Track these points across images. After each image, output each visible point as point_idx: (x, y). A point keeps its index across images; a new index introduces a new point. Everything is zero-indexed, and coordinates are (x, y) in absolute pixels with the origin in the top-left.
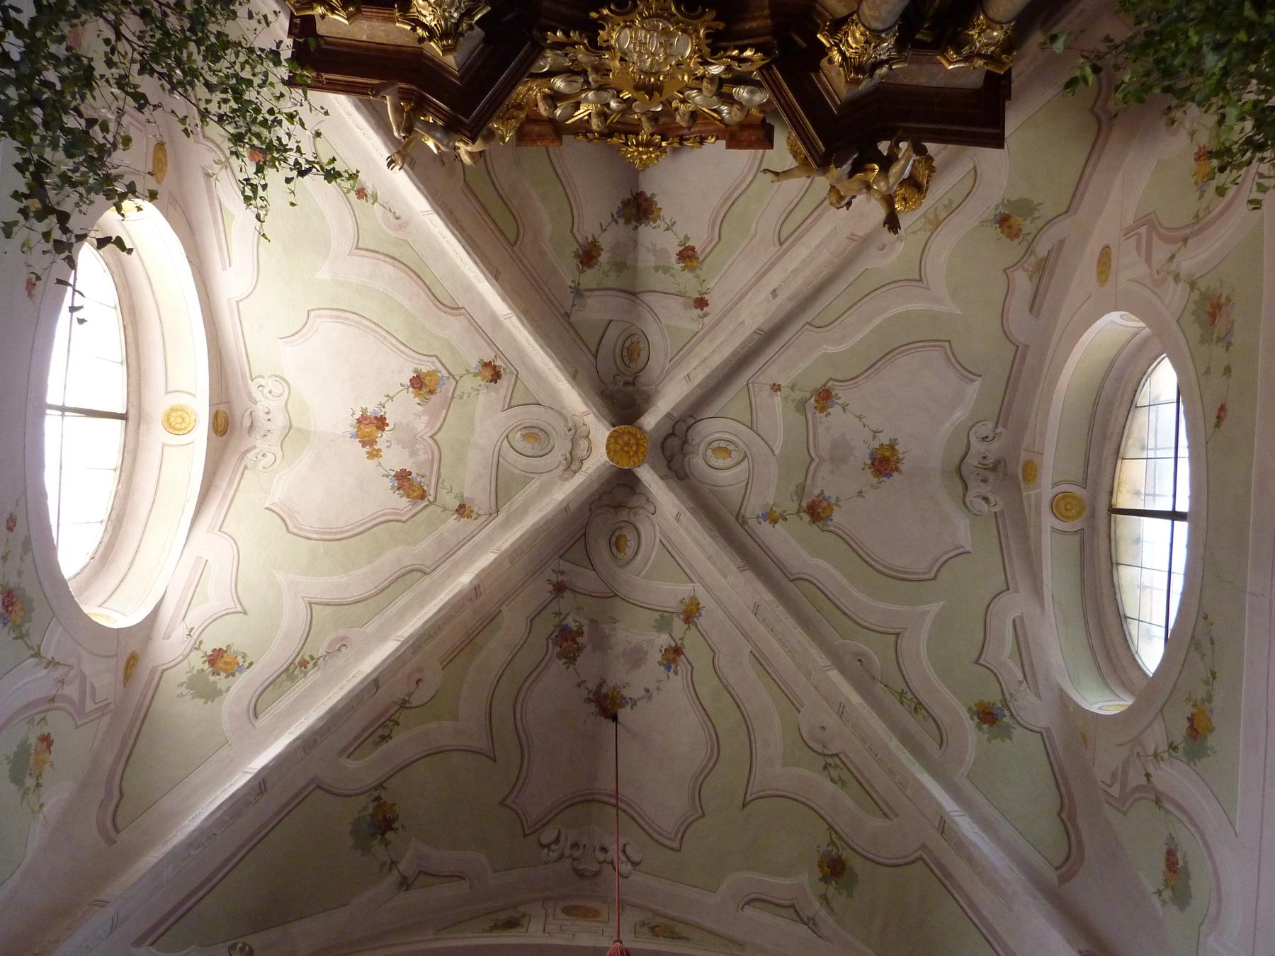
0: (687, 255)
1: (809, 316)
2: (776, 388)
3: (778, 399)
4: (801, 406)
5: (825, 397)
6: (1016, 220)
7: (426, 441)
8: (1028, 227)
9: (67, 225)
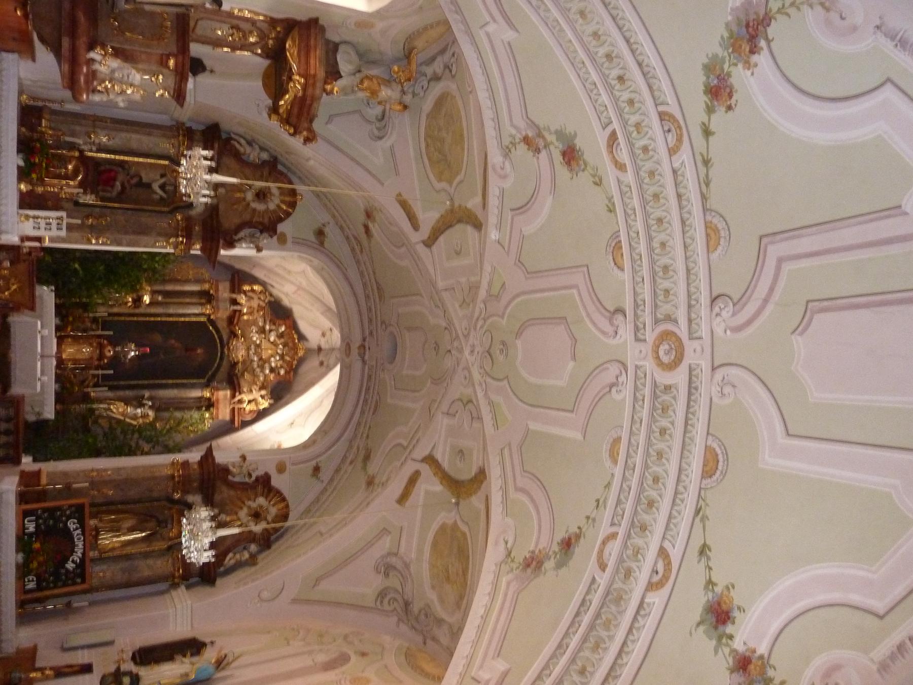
0: (323, 335)
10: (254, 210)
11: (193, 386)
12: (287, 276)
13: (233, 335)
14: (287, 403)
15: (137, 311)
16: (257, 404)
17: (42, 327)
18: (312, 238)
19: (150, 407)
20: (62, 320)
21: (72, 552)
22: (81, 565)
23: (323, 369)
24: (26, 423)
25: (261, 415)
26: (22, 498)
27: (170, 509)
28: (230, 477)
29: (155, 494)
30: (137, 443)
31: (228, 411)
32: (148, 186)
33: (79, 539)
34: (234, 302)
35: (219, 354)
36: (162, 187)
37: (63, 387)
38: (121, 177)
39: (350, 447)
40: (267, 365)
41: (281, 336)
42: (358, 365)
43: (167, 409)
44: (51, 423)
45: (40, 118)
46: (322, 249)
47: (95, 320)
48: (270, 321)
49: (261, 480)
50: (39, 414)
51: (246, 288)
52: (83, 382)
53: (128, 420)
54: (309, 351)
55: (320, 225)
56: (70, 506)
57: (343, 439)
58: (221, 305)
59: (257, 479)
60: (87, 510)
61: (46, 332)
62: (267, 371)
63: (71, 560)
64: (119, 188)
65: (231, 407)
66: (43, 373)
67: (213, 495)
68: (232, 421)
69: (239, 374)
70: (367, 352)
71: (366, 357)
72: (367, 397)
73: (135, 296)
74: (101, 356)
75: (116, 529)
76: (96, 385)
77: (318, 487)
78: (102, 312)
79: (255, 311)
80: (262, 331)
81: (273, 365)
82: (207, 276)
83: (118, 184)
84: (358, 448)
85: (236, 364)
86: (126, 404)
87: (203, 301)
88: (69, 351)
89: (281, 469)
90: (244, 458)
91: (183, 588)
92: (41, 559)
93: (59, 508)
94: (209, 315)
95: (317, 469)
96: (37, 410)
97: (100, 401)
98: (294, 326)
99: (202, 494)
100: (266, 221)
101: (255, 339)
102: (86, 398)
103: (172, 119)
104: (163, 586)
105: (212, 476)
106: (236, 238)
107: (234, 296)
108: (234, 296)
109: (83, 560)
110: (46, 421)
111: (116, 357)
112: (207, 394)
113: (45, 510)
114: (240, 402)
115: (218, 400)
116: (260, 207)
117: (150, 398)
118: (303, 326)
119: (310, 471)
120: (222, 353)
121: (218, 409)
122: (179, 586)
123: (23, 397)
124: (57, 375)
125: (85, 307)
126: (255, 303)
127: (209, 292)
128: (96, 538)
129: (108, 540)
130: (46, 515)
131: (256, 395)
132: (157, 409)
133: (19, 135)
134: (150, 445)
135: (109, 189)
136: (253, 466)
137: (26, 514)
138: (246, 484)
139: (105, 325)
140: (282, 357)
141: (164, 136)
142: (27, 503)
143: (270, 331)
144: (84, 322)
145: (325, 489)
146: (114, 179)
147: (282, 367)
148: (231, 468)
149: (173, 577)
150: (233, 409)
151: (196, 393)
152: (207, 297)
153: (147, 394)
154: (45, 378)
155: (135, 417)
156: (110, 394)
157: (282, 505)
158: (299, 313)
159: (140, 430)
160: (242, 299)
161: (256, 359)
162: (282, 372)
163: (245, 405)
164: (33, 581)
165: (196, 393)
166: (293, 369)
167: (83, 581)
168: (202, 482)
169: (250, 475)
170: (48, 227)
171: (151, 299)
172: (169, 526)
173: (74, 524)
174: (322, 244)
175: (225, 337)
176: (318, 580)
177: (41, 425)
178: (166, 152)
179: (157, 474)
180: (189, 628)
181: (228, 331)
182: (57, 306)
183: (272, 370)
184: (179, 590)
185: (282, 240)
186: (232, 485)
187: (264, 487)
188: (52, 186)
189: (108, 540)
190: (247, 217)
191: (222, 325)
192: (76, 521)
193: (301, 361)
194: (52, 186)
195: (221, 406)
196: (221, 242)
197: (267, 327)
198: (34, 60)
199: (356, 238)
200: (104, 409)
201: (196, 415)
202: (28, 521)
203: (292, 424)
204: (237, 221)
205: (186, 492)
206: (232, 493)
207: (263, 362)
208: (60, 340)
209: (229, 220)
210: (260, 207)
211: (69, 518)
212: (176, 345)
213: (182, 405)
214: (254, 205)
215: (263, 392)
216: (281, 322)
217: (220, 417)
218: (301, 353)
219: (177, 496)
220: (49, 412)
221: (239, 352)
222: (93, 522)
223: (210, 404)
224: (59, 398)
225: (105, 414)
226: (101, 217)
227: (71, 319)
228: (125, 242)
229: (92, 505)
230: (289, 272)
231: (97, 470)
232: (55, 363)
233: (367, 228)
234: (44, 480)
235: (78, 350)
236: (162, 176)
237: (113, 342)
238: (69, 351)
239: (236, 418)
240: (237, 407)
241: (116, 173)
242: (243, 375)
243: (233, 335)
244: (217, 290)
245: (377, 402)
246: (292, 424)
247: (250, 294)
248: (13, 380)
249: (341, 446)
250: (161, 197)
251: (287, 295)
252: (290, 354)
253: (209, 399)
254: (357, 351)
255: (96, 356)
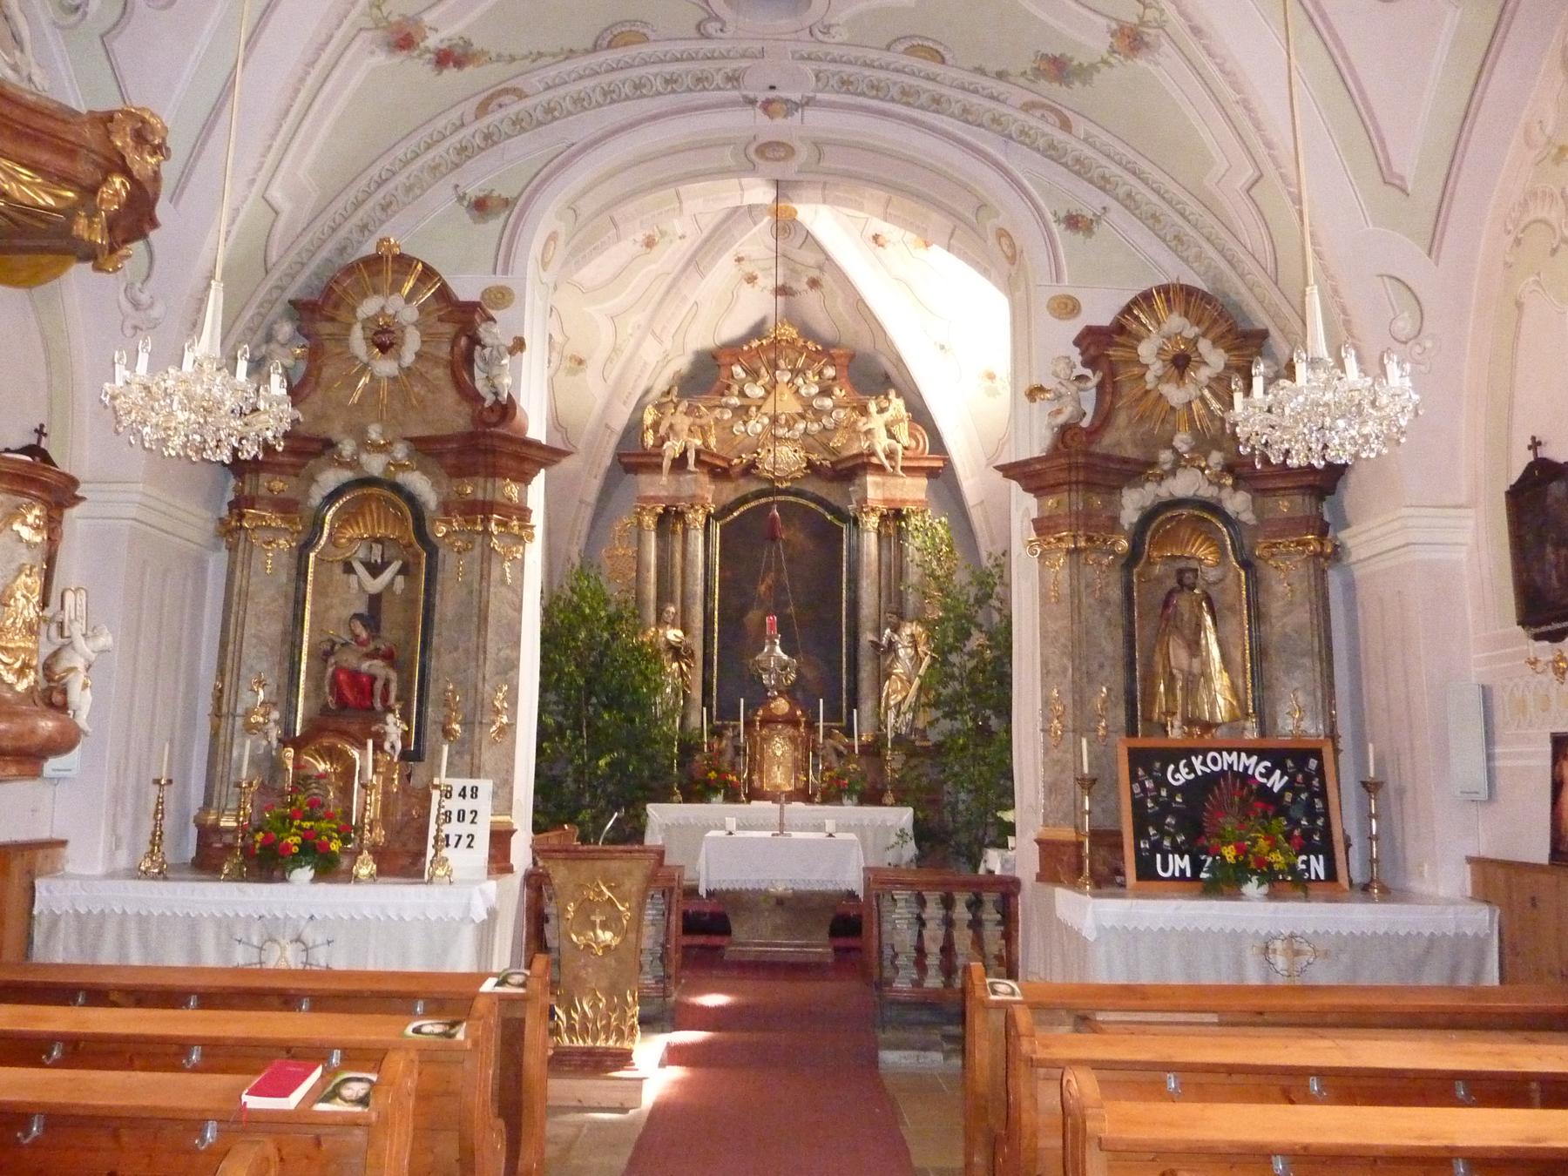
0: (751, 279)
1: (669, 279)
2: (682, 237)
3: (680, 233)
4: (663, 234)
5: (650, 243)
6: (574, 365)
7: (605, 851)
8: (568, 364)
9: (34, 960)
10: (419, 355)
11: (856, 551)
12: (623, 358)
13: (750, 470)
14: (899, 361)
15: (699, 654)
16: (896, 421)
17: (723, 827)
18: (494, 225)
19: (896, 630)
20: (716, 791)
21: (1245, 777)
22: (1277, 757)
23: (827, 279)
24: (920, 859)
25: (920, 415)
26: (1107, 881)
27: (1150, 563)
28: (1085, 423)
29: (1116, 594)
30: (971, 655)
31: (909, 481)
32: (375, 600)
33: (1215, 761)
34: (680, 463)
35: (791, 499)
36: (375, 570)
37: (850, 791)
38: (350, 659)
39: (1025, 137)
40: (816, 403)
41: (754, 374)
42: (816, 120)
43: (901, 597)
44: (920, 815)
45: (217, 830)
46: (520, 202)
47: (716, 732)
48: (723, 395)
49: (1092, 351)
50: (902, 834)
51: (650, 439)
52: (839, 754)
53: (921, 672)
54: (790, 317)
55: (462, 210)
56: (1134, 777)
57: (1001, 158)
58: (687, 490)
59: (1089, 363)
60: (1140, 742)
61: (731, 823)
62: (828, 403)
63: (1263, 780)
64: (378, 663)
65: (900, 473)
66: (819, 828)
67: (1125, 461)
68: (931, 473)
69: (834, 459)
70: (784, 94)
71: (796, 96)
72: (895, 92)
73: (666, 657)
74: (791, 721)
75: (1196, 681)
76: (848, 732)
77: (1118, 215)
78: (698, 718)
79: (698, 421)
80: (742, 412)
81: (814, 390)
82: (627, 520)
83: (365, 666)
84: (1028, 107)
85: (810, 465)
86: (888, 676)
87: (679, 527)
88: (779, 777)
89: (1067, 307)
90: (1034, 392)
91: (1343, 535)
92: (1263, 844)
93: (1138, 805)
94: (708, 516)
95: (1073, 222)
96: (893, 839)
97: (880, 724)
98: (732, 350)
99: (1120, 488)
100: (448, 329)
101: (759, 428)
102: (873, 750)
103: (217, 548)
104: (1334, 579)
105: (1081, 460)
106: (489, 400)
107: (666, 463)
108: (666, 463)
109: (1262, 754)
110: (916, 823)
111: (789, 693)
112: (872, 521)
113: (1140, 833)
114: (891, 455)
115: (885, 501)
116: (412, 343)
117: (878, 631)
118: (733, 327)
119: (1079, 237)
120: (786, 492)
121: (904, 501)
122: (1342, 546)
123: (866, 869)
124: (824, 801)
125: (689, 749)
126: (683, 422)
127: (660, 516)
128: (1208, 726)
129: (1220, 698)
130: (1152, 831)
131: (877, 422)
132: (899, 616)
133: (241, 878)
134: (974, 631)
135: (379, 685)
136: (1062, 368)
137: (1146, 872)
138: (1100, 387)
139: (729, 712)
140: (796, 372)
141: (247, 564)
142: (1119, 872)
143: (742, 394)
144: (721, 753)
145: (1130, 202)
146: (355, 675)
147: (820, 373)
148: (1061, 419)
149: (1316, 555)
150: (903, 468)
151: (870, 542)
152: (670, 519)
153: (867, 637)
154: (830, 826)
155: (917, 660)
156: (867, 706)
157: (1159, 303)
158: (703, 337)
159: (942, 654)
160: (672, 448)
161: (801, 426)
162: (830, 372)
163: (899, 448)
164: (1307, 863)
165: (870, 542)
166: (827, 351)
167: (1317, 754)
168: (1090, 486)
169: (1080, 378)
170: (469, 817)
171: (674, 626)
172: (1193, 564)
173: (1177, 770)
174: (507, 203)
175: (754, 487)
176: (1390, 180)
177: (923, 832)
178: (285, 559)
179: (1065, 589)
180: (1471, 512)
181: (742, 481)
182: (689, 798)
183: (826, 392)
184: (1350, 544)
185: (502, 296)
186: (1104, 418)
187: (1111, 344)
188: (366, 805)
189: (1220, 698)
190: (440, 374)
191: (729, 492)
192: (1172, 767)
193: (807, 332)
194: (366, 805)
195: (898, 495)
196: (500, 430)
197: (735, 401)
198: (63, 843)
199: (483, 109)
200: (898, 716)
201: (913, 544)
202: (1165, 869)
203: (942, 347)
204: (450, 397)
205: (1114, 523)
206: (1121, 419)
207: (809, 410)
208: (755, 794)
209: (452, 417)
210: (412, 343)
211: (1162, 782)
212: (769, 581)
213: (894, 571)
214: (408, 358)
215: (873, 407)
216: (724, 372)
217: (922, 496)
218: (792, 333)
219: (1124, 544)
220: (903, 817)
221: (786, 458)
222: (1176, 733)
223: (895, 516)
224: (871, 797)
225: (909, 716)
226: (446, 704)
227: (713, 775)
228: (505, 653)
229: (1132, 732)
230: (616, 350)
231: (1047, 719)
232: (798, 805)
233: (444, 59)
234: (1066, 834)
235: (779, 764)
236: (348, 569)
237: (760, 697)
238: (779, 777)
239: (926, 464)
240: (900, 463)
241: (339, 669)
242: (834, 452)
243: (750, 470)
244: (657, 499)
245: (912, 51)
246: (942, 347)
247: (662, 431)
248: (830, 887)
249: (1021, 162)
250: (400, 572)
251: (666, 359)
252: (792, 356)
253: (883, 517)
254: (779, 121)
255: (790, 731)
